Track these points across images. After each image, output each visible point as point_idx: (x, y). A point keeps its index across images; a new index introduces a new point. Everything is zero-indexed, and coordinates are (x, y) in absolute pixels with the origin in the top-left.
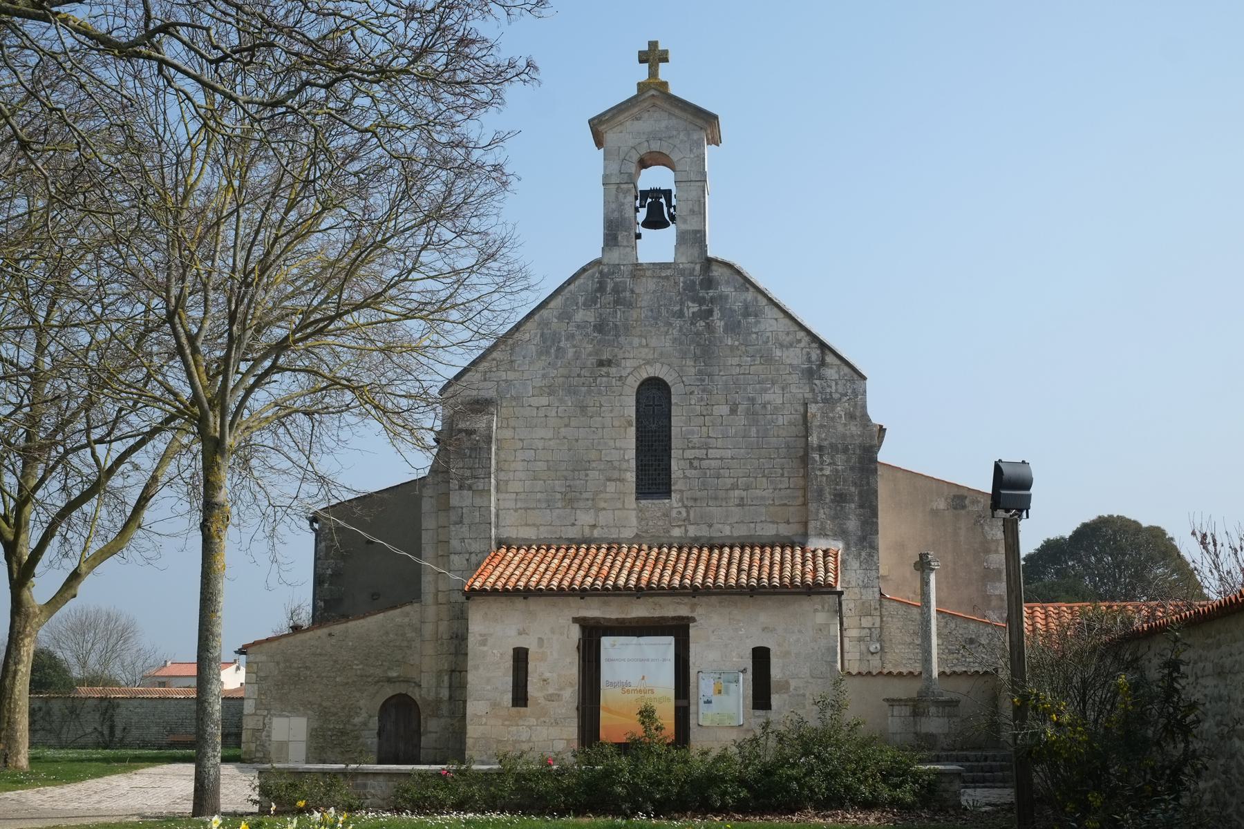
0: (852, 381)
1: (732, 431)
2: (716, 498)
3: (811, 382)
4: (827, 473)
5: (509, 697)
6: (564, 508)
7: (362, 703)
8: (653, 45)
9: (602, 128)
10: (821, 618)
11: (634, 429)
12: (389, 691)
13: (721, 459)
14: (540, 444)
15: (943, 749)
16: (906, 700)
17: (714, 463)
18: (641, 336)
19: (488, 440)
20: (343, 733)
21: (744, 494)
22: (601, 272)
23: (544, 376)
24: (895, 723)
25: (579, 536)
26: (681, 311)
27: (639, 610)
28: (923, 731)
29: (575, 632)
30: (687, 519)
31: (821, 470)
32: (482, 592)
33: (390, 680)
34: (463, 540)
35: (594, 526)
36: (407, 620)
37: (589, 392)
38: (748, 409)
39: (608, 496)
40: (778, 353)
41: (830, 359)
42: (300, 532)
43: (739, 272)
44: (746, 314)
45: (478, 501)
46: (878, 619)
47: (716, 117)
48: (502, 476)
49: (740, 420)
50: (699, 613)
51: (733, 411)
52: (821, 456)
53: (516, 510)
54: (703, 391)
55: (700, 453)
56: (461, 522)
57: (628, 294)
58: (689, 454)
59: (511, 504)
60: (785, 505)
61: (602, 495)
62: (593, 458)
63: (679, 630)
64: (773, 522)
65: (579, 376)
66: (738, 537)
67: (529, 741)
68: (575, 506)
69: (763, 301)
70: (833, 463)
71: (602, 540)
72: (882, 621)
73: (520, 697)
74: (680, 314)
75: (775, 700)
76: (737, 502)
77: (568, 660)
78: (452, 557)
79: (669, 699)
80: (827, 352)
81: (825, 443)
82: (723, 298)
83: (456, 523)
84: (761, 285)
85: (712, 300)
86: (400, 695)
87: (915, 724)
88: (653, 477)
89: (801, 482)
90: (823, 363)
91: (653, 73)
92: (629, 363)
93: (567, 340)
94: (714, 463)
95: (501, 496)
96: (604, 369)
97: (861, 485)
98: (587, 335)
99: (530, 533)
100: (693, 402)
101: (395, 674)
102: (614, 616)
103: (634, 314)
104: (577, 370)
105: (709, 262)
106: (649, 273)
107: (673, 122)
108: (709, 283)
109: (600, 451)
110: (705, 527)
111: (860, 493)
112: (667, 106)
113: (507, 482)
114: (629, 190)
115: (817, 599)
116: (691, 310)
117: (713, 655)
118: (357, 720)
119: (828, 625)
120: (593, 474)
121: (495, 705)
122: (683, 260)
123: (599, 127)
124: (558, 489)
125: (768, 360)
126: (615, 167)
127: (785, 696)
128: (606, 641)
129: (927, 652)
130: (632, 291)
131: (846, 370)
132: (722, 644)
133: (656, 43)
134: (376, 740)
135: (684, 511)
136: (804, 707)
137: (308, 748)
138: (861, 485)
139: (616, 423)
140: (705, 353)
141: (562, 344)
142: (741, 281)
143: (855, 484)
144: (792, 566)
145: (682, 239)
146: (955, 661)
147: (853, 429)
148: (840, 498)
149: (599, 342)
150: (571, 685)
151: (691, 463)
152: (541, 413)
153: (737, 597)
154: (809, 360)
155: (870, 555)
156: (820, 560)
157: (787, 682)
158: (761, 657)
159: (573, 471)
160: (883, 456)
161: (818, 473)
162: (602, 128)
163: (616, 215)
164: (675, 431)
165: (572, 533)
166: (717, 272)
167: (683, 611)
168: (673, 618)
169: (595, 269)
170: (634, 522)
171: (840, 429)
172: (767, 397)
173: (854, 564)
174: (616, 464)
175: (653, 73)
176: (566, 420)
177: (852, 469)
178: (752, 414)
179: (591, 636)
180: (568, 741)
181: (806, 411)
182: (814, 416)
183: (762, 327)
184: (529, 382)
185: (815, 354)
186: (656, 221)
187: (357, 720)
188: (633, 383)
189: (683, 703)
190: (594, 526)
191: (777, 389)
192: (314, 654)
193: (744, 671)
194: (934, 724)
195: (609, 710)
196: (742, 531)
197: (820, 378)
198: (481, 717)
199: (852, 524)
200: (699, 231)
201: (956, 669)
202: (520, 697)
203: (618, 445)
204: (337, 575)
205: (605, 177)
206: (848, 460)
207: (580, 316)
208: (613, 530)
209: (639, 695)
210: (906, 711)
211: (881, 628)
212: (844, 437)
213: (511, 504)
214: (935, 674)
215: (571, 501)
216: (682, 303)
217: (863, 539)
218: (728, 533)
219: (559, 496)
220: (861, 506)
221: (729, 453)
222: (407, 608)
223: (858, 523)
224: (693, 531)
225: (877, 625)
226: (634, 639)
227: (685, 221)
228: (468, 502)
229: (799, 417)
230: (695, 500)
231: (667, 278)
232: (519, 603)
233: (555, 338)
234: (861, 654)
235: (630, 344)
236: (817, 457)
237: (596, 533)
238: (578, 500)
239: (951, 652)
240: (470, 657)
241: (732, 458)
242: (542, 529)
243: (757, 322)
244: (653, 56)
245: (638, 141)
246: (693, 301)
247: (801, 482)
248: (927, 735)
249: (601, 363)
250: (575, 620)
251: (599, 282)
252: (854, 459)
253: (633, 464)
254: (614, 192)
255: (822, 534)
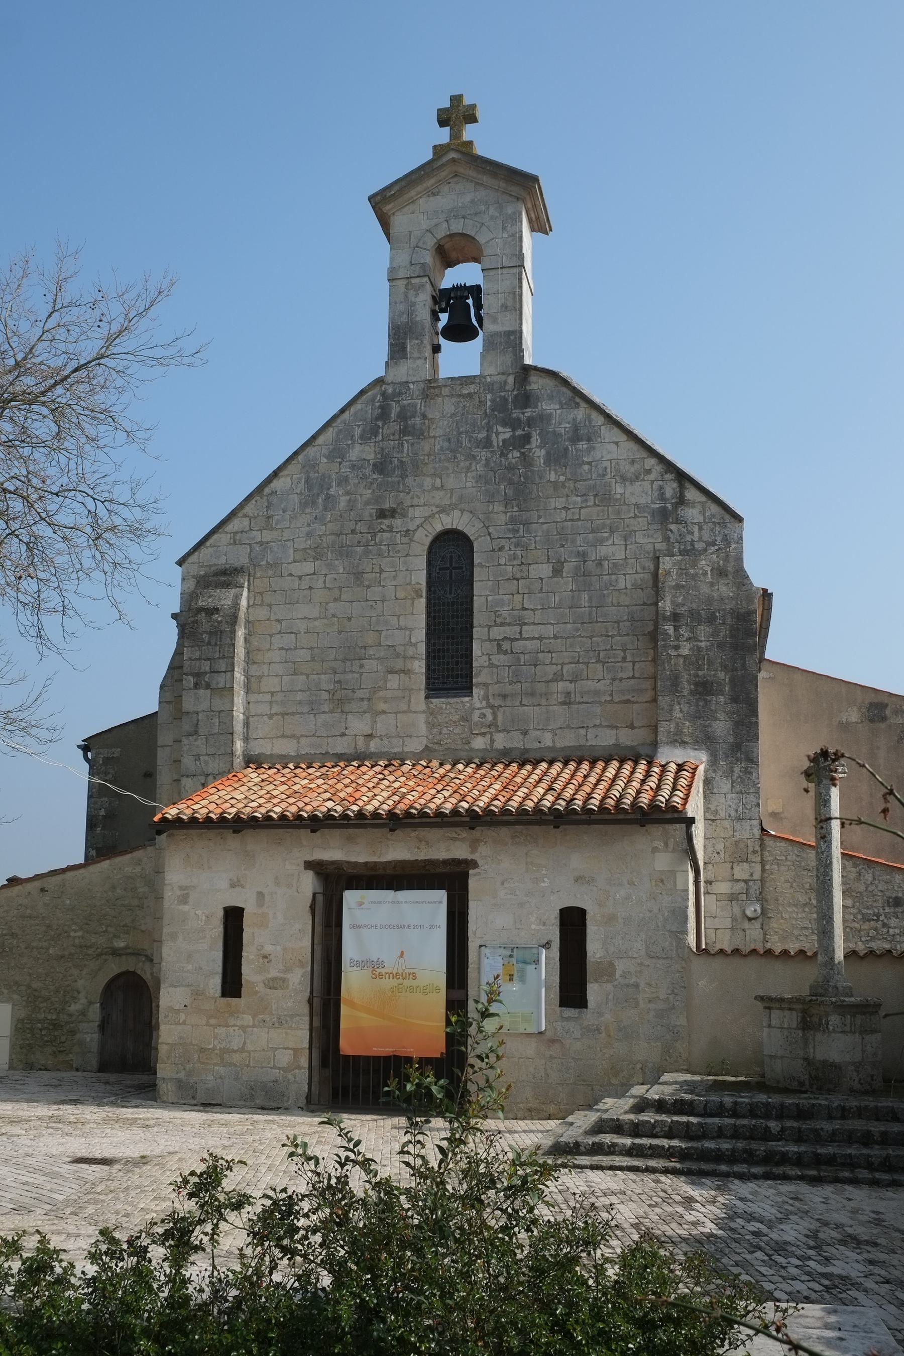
0: (723, 524)
1: (554, 600)
2: (533, 694)
3: (664, 528)
4: (685, 651)
5: (215, 983)
6: (331, 712)
7: (81, 983)
8: (456, 100)
9: (387, 208)
10: (663, 861)
11: (423, 601)
12: (114, 968)
13: (540, 638)
14: (302, 626)
15: (852, 1091)
16: (790, 1001)
17: (530, 645)
18: (434, 475)
19: (233, 620)
20: (56, 1025)
21: (571, 687)
22: (384, 394)
23: (309, 535)
24: (774, 1038)
25: (350, 750)
26: (488, 438)
27: (397, 850)
28: (820, 1056)
29: (308, 883)
30: (493, 724)
31: (677, 648)
32: (178, 822)
33: (115, 953)
34: (197, 757)
35: (370, 736)
36: (138, 869)
37: (367, 553)
38: (577, 568)
39: (389, 694)
40: (620, 490)
41: (691, 494)
42: (14, 753)
43: (565, 382)
44: (576, 438)
45: (218, 704)
46: (758, 867)
47: (535, 179)
48: (254, 670)
49: (567, 583)
50: (483, 854)
51: (557, 572)
52: (676, 628)
53: (271, 716)
54: (517, 545)
55: (509, 631)
56: (196, 733)
57: (418, 420)
58: (497, 633)
59: (264, 709)
60: (628, 701)
61: (382, 694)
62: (370, 642)
63: (453, 880)
64: (610, 727)
65: (353, 532)
66: (563, 749)
67: (242, 1050)
68: (347, 708)
69: (599, 420)
70: (693, 638)
71: (381, 755)
72: (763, 870)
73: (232, 984)
74: (487, 443)
75: (593, 992)
76: (561, 698)
77: (298, 926)
78: (184, 781)
79: (438, 989)
80: (687, 485)
81: (682, 610)
82: (544, 418)
83: (190, 735)
84: (597, 399)
85: (530, 422)
86: (127, 973)
87: (806, 1042)
88: (449, 671)
89: (649, 669)
90: (681, 501)
91: (456, 135)
92: (418, 512)
93: (339, 485)
94: (530, 645)
95: (253, 698)
96: (387, 522)
97: (734, 669)
98: (364, 477)
99: (286, 747)
100: (502, 561)
101: (122, 945)
102: (362, 859)
103: (426, 446)
104: (352, 525)
105: (527, 370)
106: (445, 391)
107: (482, 193)
108: (525, 399)
109: (379, 632)
110: (517, 735)
111: (733, 681)
112: (472, 173)
113: (260, 678)
114: (422, 286)
115: (656, 830)
116: (502, 437)
117: (502, 920)
118: (74, 1008)
119: (673, 873)
120: (370, 665)
121: (198, 994)
122: (491, 370)
123: (383, 204)
124: (325, 686)
125: (605, 499)
126: (404, 258)
127: (609, 987)
128: (350, 897)
129: (826, 917)
130: (424, 416)
131: (714, 508)
132: (515, 902)
133: (461, 96)
134: (96, 1036)
135: (489, 712)
136: (637, 1005)
137: (12, 1047)
138: (734, 669)
139: (401, 594)
140: (519, 492)
141: (332, 491)
142: (569, 393)
143: (725, 668)
144: (626, 785)
145: (489, 345)
146: (872, 933)
147: (723, 589)
148: (704, 689)
149: (380, 486)
150: (302, 965)
151: (499, 646)
152: (305, 584)
153: (536, 828)
154: (662, 497)
155: (747, 772)
156: (670, 777)
157: (611, 965)
158: (573, 922)
159: (344, 661)
160: (776, 649)
161: (672, 652)
162: (387, 208)
163: (405, 318)
164: (478, 602)
165: (341, 746)
166: (536, 384)
167: (460, 852)
168: (446, 862)
169: (376, 390)
170: (423, 729)
171: (705, 589)
172: (603, 551)
173: (725, 785)
174: (400, 649)
175: (456, 135)
176: (336, 591)
177: (721, 646)
178: (582, 575)
179: (335, 882)
180: (296, 1051)
181: (657, 568)
182: (668, 573)
183: (597, 454)
184: (289, 544)
185: (671, 488)
186: (460, 331)
187: (74, 1008)
188: (424, 538)
189: (457, 994)
190: (370, 736)
191: (618, 540)
192: (23, 917)
193: (547, 945)
194: (837, 1046)
195: (352, 1004)
196: (568, 740)
197: (677, 521)
198: (178, 1011)
199: (721, 726)
200: (513, 332)
201: (874, 945)
202: (232, 984)
203: (402, 623)
204: (111, 816)
205: (392, 270)
206: (715, 633)
207: (356, 452)
208: (395, 741)
209: (394, 982)
210: (791, 1019)
211: (762, 880)
212: (710, 600)
213: (264, 709)
214: (839, 955)
215: (341, 701)
216: (489, 429)
217: (736, 747)
218: (549, 743)
219: (325, 696)
220: (734, 700)
221: (550, 631)
222: (139, 854)
223: (729, 725)
224: (501, 741)
225: (757, 876)
226: (389, 895)
227: (495, 321)
228: (205, 705)
229: (648, 577)
230: (505, 697)
231: (470, 395)
232: (233, 841)
233: (324, 483)
234: (734, 919)
235: (421, 486)
236: (670, 629)
237: (373, 746)
238: (350, 700)
239: (866, 919)
240: (166, 921)
241: (555, 637)
242: (303, 741)
243: (591, 449)
244: (457, 114)
245: (435, 221)
246: (504, 425)
247: (649, 669)
248: (824, 1063)
249: (382, 514)
250: (309, 865)
251: (381, 407)
252: (724, 632)
253: (422, 649)
254: (403, 289)
255: (678, 741)
